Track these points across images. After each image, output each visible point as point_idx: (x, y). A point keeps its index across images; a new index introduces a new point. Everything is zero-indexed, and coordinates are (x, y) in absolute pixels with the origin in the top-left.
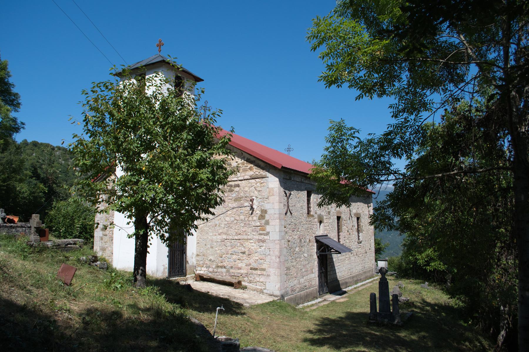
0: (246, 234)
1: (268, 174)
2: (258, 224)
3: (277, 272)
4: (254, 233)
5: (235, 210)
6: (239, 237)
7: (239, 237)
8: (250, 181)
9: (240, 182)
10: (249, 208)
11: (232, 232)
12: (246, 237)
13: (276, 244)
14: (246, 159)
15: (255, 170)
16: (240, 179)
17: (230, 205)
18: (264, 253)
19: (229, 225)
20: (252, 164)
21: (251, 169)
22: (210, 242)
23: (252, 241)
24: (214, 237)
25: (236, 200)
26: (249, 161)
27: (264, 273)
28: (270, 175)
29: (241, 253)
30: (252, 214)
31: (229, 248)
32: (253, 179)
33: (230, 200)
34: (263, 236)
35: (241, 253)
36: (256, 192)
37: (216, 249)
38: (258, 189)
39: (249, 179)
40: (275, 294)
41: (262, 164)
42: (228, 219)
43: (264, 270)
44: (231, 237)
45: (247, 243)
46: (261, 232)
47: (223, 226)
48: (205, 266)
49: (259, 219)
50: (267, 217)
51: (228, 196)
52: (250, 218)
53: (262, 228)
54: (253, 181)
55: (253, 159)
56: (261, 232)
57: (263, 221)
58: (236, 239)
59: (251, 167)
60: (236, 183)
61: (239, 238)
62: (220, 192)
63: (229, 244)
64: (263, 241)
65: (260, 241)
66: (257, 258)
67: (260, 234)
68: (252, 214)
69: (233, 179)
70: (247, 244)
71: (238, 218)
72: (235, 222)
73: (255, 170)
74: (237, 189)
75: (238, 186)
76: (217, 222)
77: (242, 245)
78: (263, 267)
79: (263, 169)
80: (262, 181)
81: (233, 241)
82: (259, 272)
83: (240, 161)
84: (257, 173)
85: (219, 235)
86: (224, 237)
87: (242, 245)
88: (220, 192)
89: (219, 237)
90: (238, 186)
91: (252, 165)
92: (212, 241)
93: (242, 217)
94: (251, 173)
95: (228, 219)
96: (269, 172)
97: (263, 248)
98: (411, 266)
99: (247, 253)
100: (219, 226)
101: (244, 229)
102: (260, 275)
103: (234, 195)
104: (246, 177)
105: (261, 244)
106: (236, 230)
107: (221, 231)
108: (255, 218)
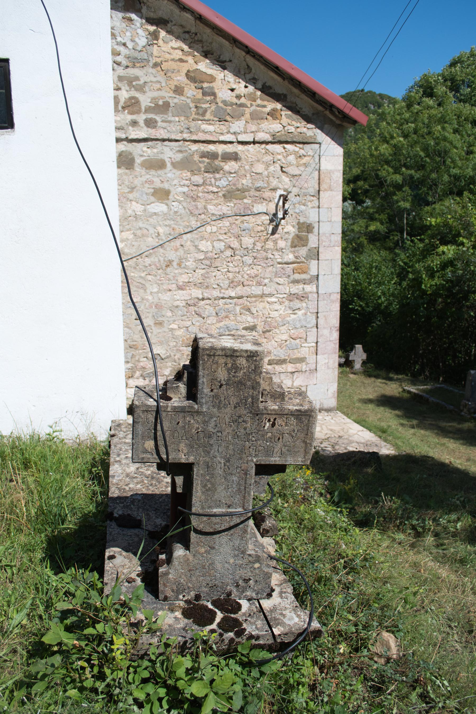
0: (259, 284)
1: (321, 136)
2: (291, 257)
3: (331, 362)
4: (281, 280)
5: (226, 223)
6: (239, 291)
7: (239, 291)
8: (270, 147)
9: (240, 147)
10: (266, 218)
11: (218, 277)
12: (257, 290)
13: (333, 301)
14: (260, 86)
15: (285, 120)
16: (242, 138)
17: (210, 207)
18: (304, 323)
19: (210, 262)
20: (278, 100)
21: (273, 114)
22: (154, 310)
23: (273, 299)
24: (166, 297)
25: (229, 195)
26: (267, 91)
27: (304, 367)
28: (328, 139)
29: (246, 329)
30: (273, 233)
31: (212, 320)
32: (280, 142)
33: (211, 196)
34: (301, 286)
35: (246, 329)
36: (286, 179)
37: (174, 326)
38: (292, 170)
39: (267, 143)
40: (326, 406)
41: (305, 102)
42: (205, 245)
43: (302, 360)
44: (216, 293)
45: (261, 306)
46: (297, 276)
47: (190, 264)
48: (138, 374)
49: (293, 246)
50: (313, 241)
51: (204, 183)
52: (270, 244)
53: (300, 266)
54: (278, 148)
55: (261, 59)
56: (297, 276)
57: (303, 251)
58: (230, 298)
59: (274, 110)
60: (229, 148)
61: (240, 293)
62: (245, 224)
63: (209, 310)
64: (302, 297)
65: (292, 297)
66: (285, 337)
67: (296, 282)
68: (273, 233)
69: (222, 138)
70: (259, 307)
71: (235, 244)
72: (229, 253)
73: (285, 120)
74: (230, 166)
75: (235, 157)
76: (172, 255)
77: (249, 310)
78: (299, 355)
79: (308, 120)
80: (302, 152)
81: (222, 301)
82: (290, 367)
83: (241, 87)
84: (292, 129)
85: (180, 288)
86: (197, 293)
87: (249, 310)
88: (245, 224)
89: (182, 295)
90: (235, 157)
91: (279, 106)
92: (158, 306)
93: (248, 241)
94: (275, 126)
95: (205, 245)
96: (322, 129)
97: (300, 313)
98: (414, 214)
99: (260, 329)
100: (179, 265)
101: (253, 272)
102: (293, 373)
103: (223, 183)
104: (261, 136)
105: (297, 304)
106: (231, 275)
107: (183, 279)
108: (282, 244)
